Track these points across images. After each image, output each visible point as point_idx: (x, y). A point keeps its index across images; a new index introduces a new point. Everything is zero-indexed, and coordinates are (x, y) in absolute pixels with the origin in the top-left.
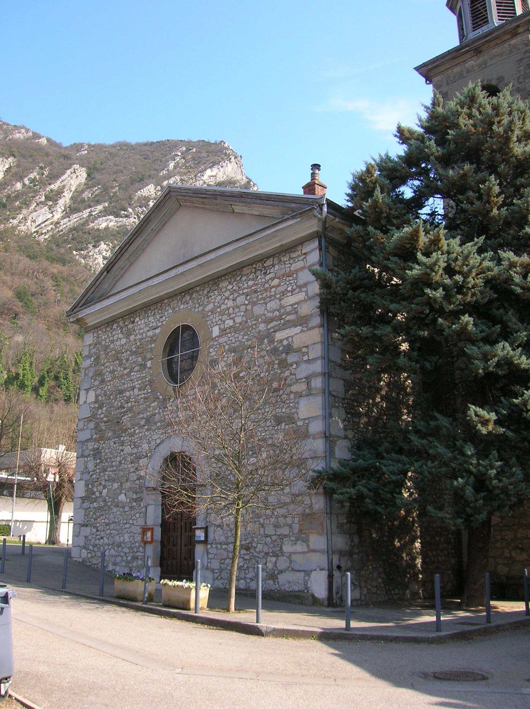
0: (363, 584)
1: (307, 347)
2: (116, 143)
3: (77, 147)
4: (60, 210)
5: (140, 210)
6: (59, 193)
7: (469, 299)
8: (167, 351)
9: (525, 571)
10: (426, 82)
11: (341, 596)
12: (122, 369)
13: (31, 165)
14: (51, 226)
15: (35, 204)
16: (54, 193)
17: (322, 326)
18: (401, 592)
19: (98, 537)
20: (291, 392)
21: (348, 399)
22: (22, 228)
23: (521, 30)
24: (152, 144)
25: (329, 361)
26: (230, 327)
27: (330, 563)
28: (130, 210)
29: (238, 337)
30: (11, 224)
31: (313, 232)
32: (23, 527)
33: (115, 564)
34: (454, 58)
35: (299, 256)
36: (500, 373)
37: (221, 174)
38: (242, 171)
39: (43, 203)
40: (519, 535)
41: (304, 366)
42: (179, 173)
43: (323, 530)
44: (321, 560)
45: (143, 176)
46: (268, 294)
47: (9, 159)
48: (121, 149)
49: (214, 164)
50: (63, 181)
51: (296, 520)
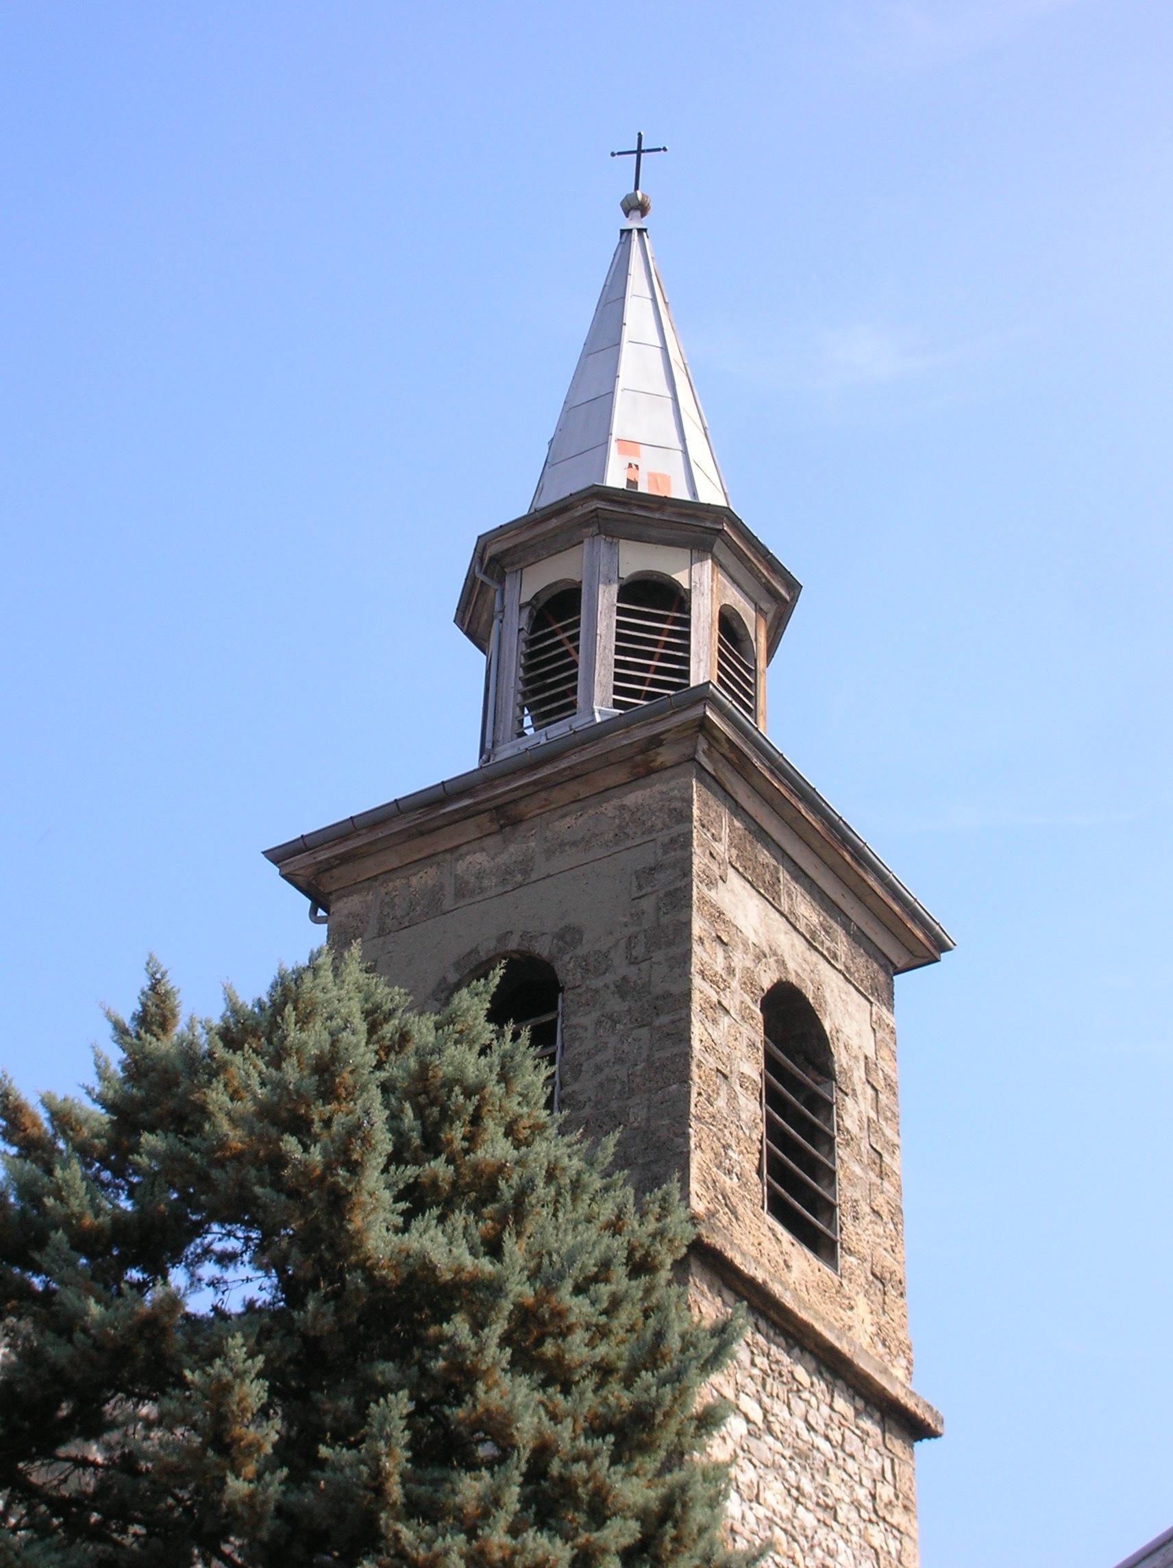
10: (313, 912)
23: (665, 756)
34: (420, 832)
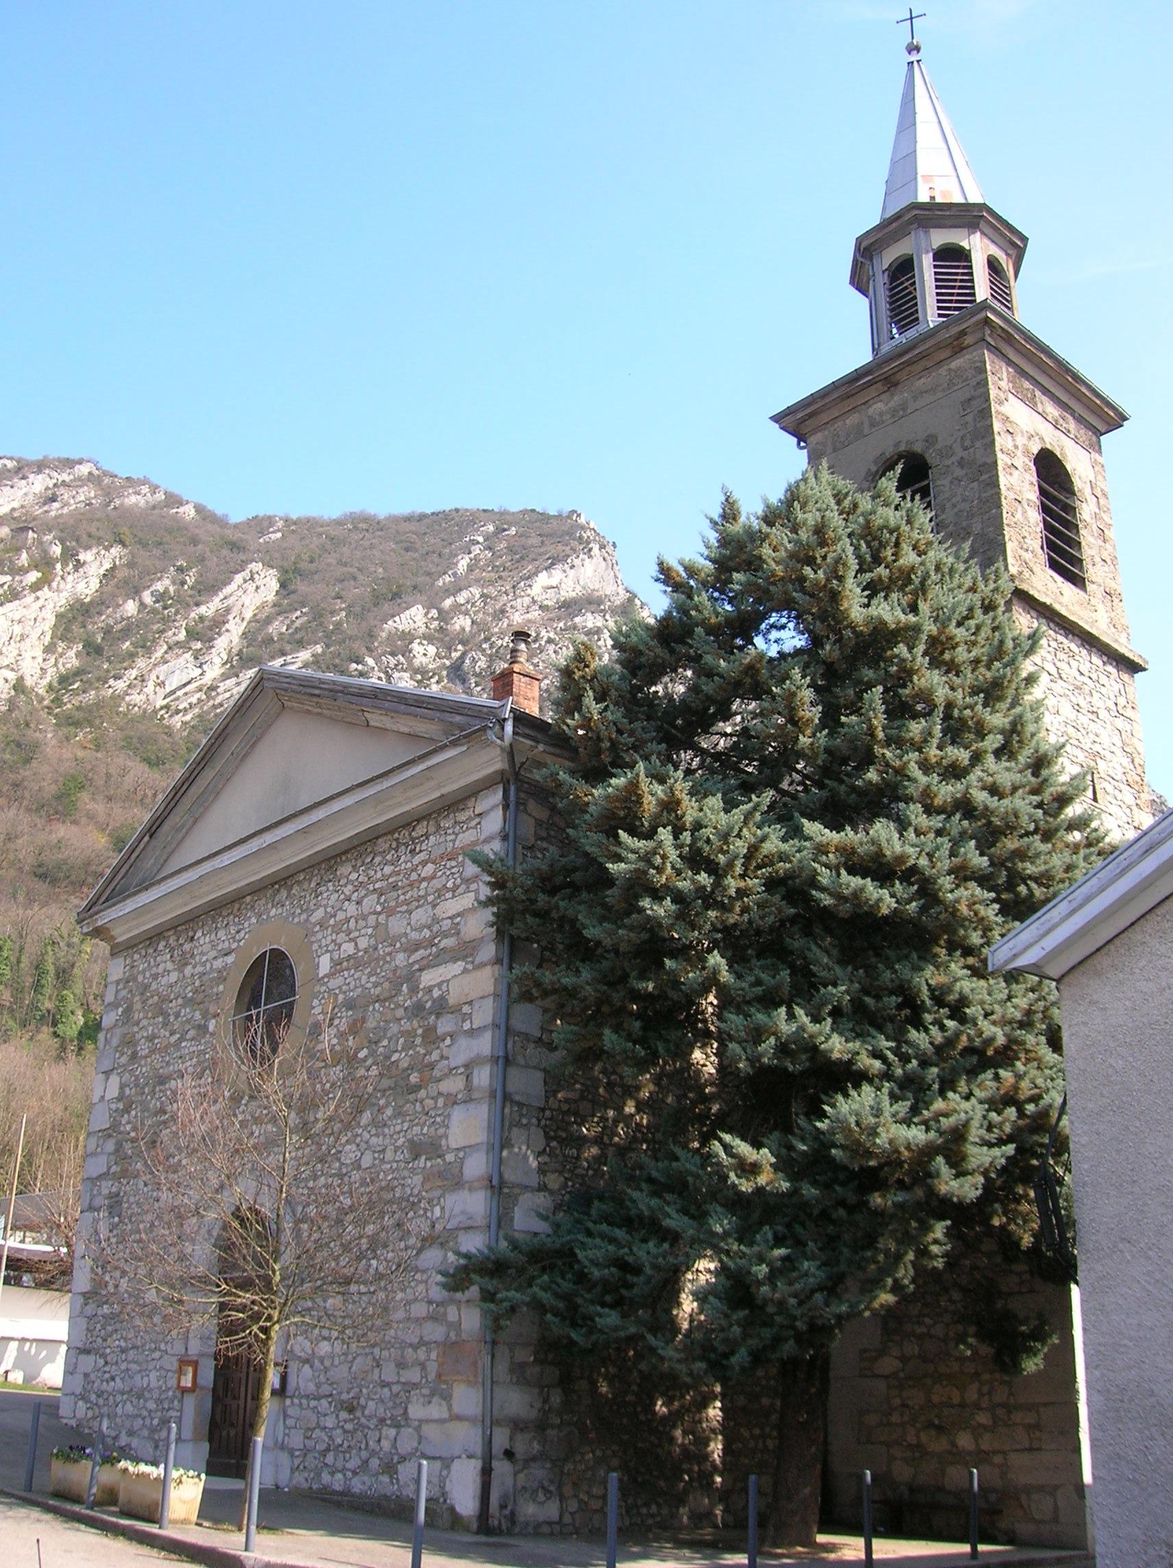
0: (568, 1490)
1: (470, 1003)
2: (345, 516)
3: (261, 524)
4: (217, 661)
5: (393, 661)
6: (218, 623)
7: (732, 919)
8: (247, 1000)
9: (865, 1474)
11: (513, 1513)
12: (167, 1034)
13: (157, 563)
14: (198, 695)
15: (165, 647)
16: (207, 623)
17: (498, 961)
18: (665, 1511)
19: (107, 1376)
20: (440, 1094)
21: (552, 1110)
22: (136, 698)
24: (422, 517)
25: (509, 1031)
26: (350, 957)
27: (488, 1443)
28: (370, 661)
29: (360, 979)
30: (111, 690)
31: (495, 772)
32: (38, 1353)
33: (131, 1433)
35: (470, 819)
36: (791, 1068)
37: (571, 583)
38: (616, 577)
39: (183, 646)
40: (936, 1399)
41: (463, 1042)
42: (477, 581)
43: (475, 1376)
44: (468, 1436)
45: (399, 587)
46: (415, 893)
47: (112, 550)
48: (356, 528)
49: (555, 561)
50: (225, 598)
51: (433, 1355)
